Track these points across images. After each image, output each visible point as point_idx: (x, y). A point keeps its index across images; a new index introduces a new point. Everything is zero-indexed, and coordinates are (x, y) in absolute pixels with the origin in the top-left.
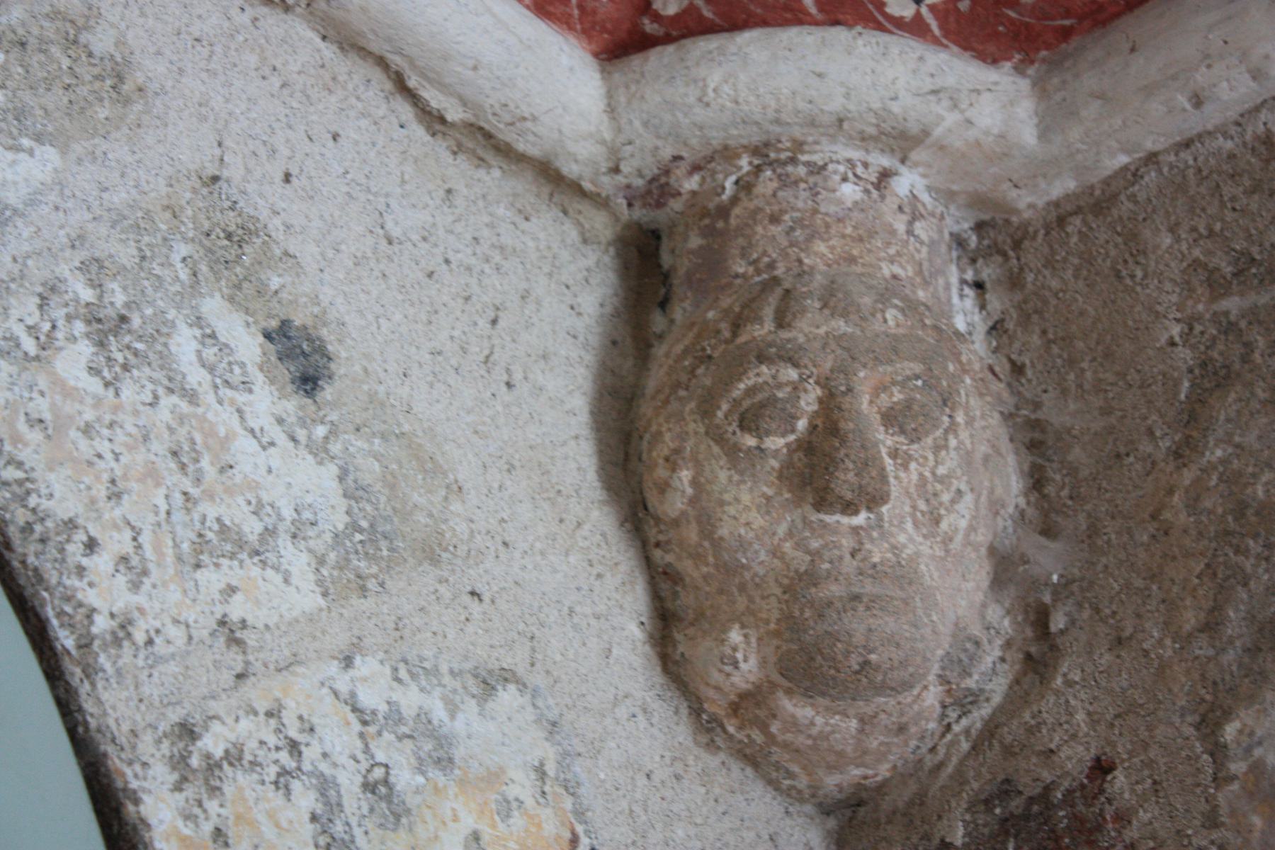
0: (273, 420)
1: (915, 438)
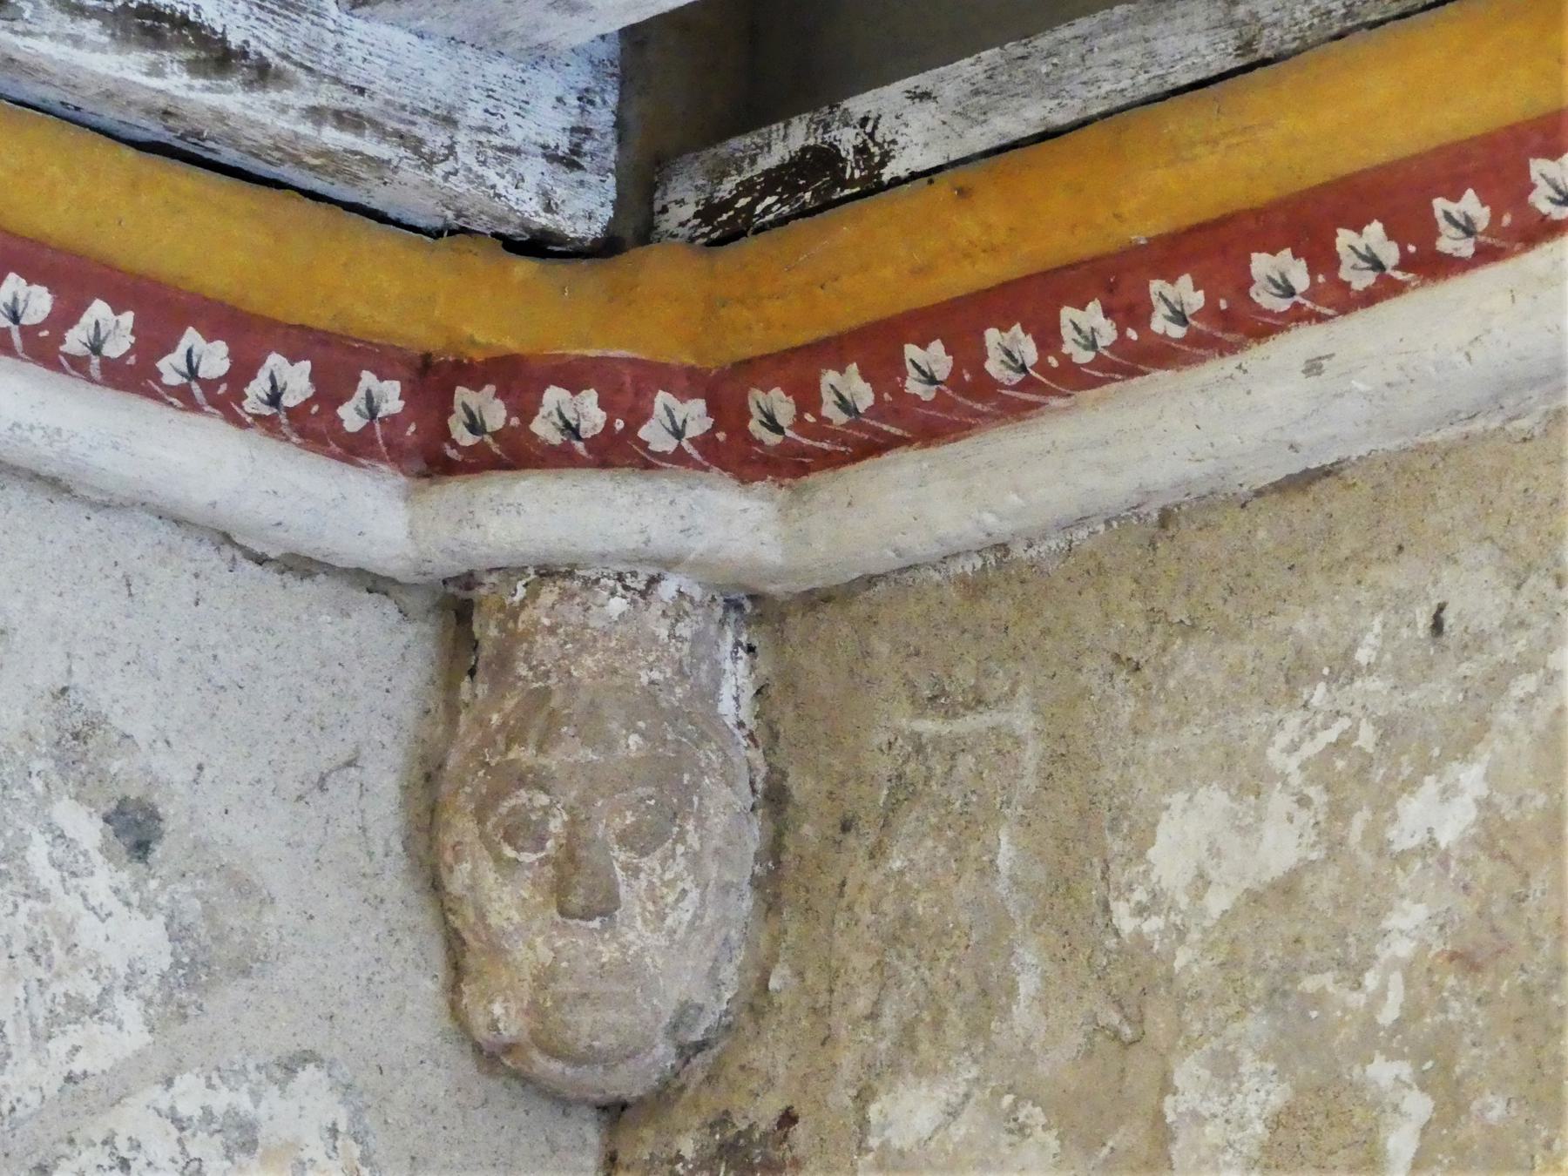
0: (110, 892)
1: (644, 853)
